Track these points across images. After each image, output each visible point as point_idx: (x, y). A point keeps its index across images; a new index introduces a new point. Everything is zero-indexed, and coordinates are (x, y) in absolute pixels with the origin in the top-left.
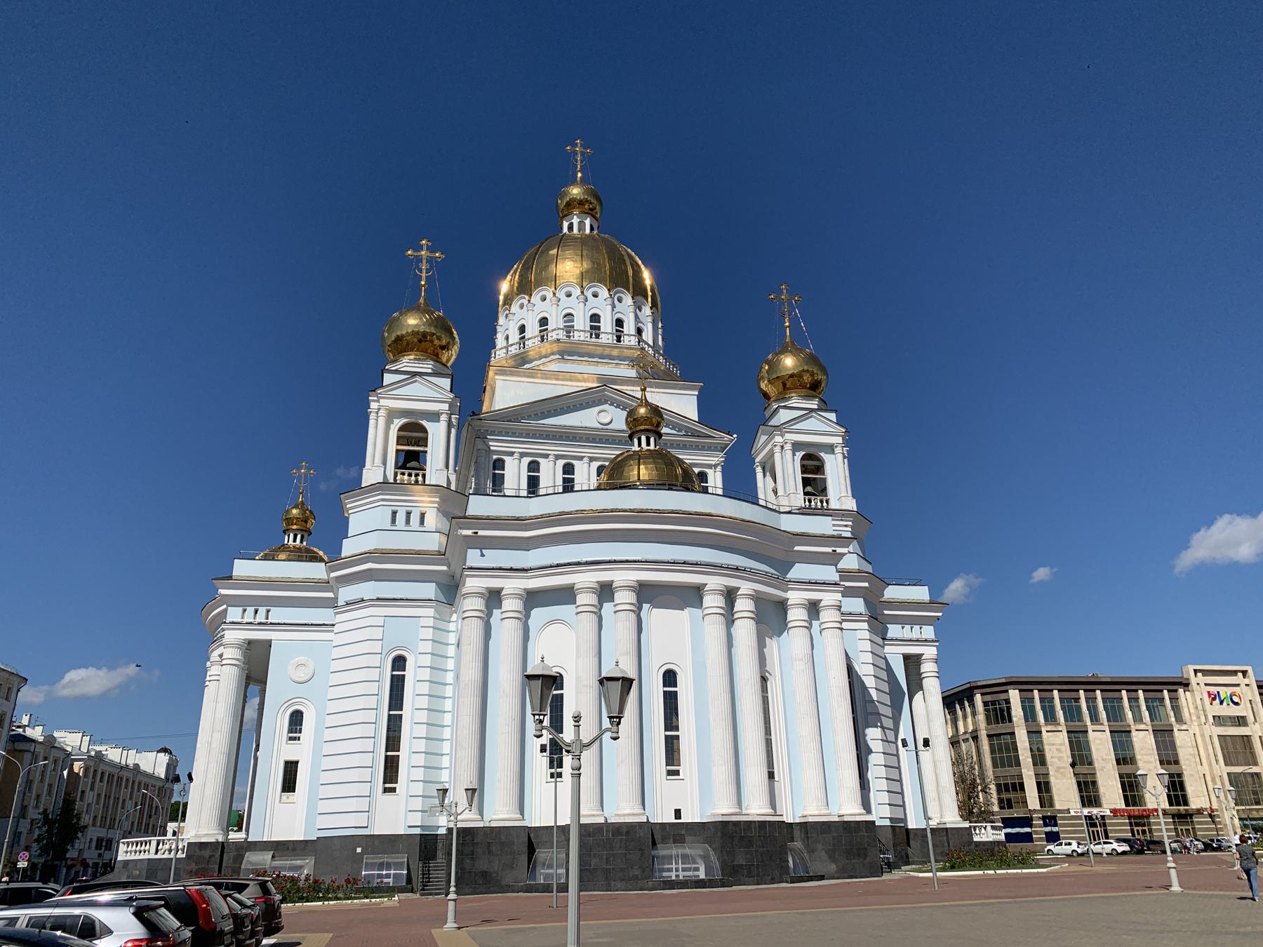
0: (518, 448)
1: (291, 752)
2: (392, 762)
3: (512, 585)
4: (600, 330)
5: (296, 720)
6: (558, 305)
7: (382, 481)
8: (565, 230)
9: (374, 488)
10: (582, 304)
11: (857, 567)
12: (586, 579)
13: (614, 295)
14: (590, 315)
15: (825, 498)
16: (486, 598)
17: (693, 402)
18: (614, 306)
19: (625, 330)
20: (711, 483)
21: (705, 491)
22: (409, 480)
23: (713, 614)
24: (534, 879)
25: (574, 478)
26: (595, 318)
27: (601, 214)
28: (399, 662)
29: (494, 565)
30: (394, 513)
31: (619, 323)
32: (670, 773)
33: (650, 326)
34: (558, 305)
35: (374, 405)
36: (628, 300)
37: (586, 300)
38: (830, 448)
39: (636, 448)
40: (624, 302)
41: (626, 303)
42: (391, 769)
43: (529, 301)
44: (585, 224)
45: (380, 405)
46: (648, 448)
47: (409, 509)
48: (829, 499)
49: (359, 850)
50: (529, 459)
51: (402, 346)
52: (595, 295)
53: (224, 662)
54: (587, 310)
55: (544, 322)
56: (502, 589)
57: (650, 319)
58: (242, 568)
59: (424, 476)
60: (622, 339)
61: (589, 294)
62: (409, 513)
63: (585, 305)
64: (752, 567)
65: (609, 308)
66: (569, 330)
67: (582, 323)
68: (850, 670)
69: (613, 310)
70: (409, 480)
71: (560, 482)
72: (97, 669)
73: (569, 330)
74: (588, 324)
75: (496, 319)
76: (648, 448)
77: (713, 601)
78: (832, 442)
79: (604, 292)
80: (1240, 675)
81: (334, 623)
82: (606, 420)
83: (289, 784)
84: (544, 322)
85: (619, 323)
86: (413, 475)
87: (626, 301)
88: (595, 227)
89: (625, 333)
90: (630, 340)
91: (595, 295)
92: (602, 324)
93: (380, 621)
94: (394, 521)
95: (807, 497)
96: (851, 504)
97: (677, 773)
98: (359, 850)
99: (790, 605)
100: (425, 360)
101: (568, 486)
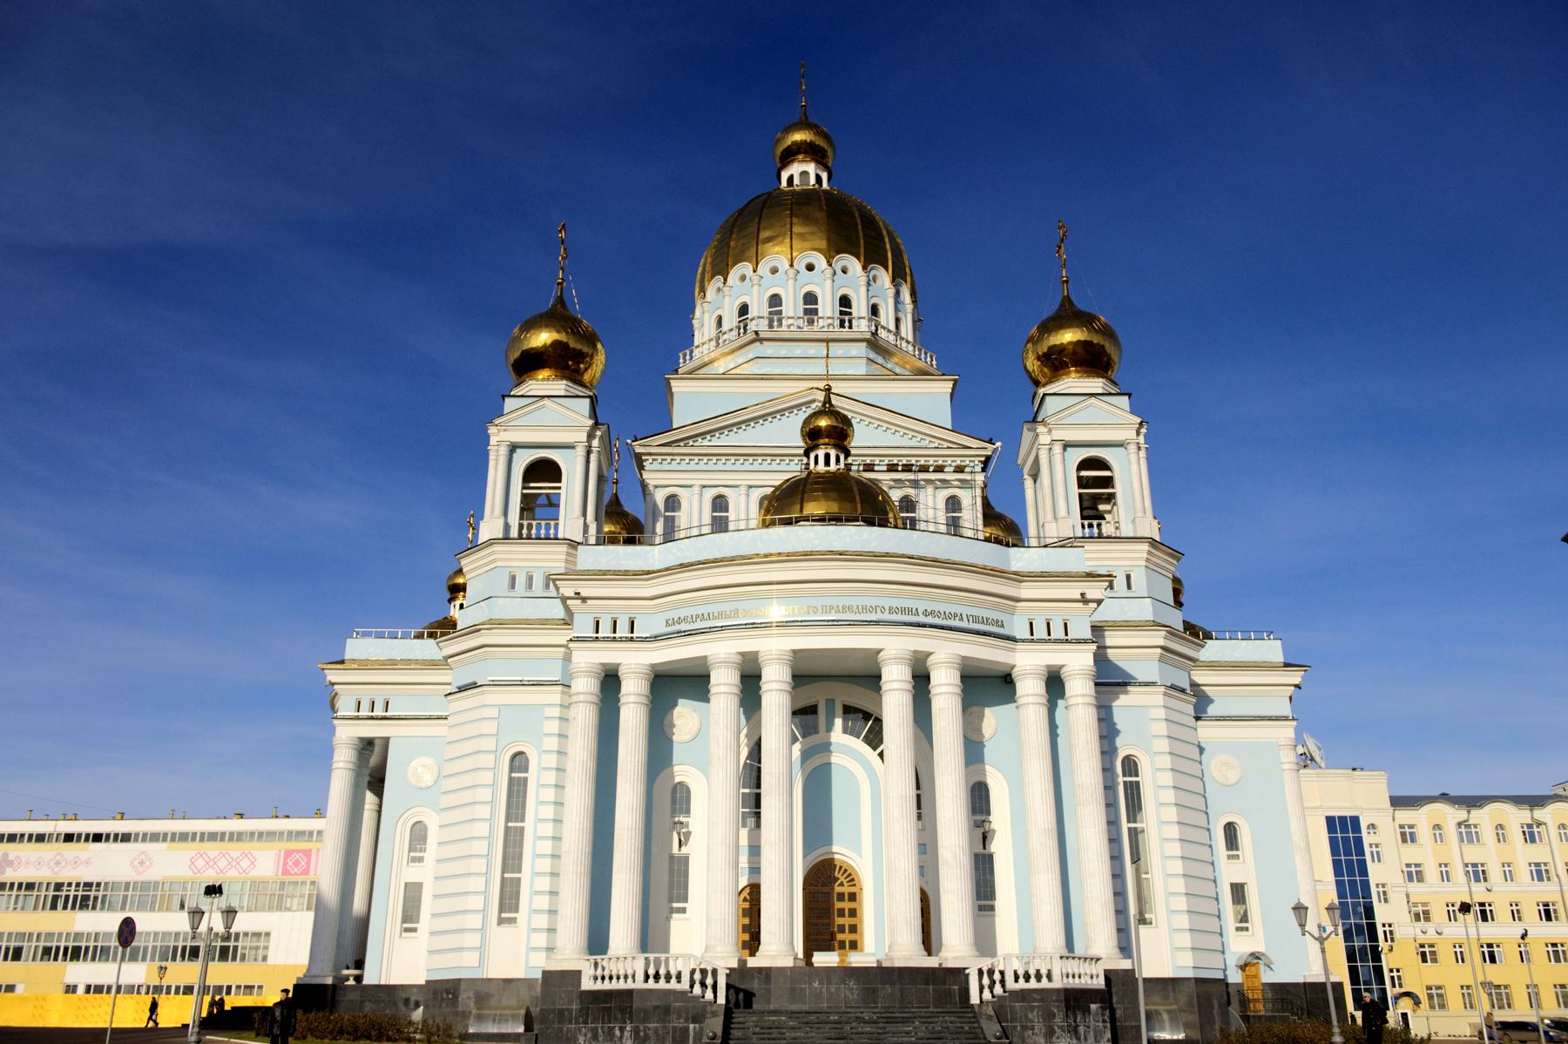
0: (697, 480)
1: (413, 874)
2: (1232, 844)
4: (816, 313)
5: (1231, 831)
6: (760, 285)
7: (501, 536)
8: (784, 183)
9: (491, 542)
14: (802, 294)
19: (854, 311)
20: (921, 513)
21: (912, 524)
22: (1091, 532)
25: (727, 517)
27: (834, 160)
34: (760, 285)
35: (493, 441)
36: (884, 277)
42: (509, 899)
45: (499, 437)
46: (827, 468)
50: (714, 492)
51: (528, 364)
52: (810, 268)
55: (775, 300)
58: (357, 648)
59: (556, 526)
63: (834, 281)
65: (829, 282)
70: (1091, 532)
71: (707, 519)
72: (1117, 735)
74: (801, 307)
75: (693, 312)
79: (854, 265)
81: (444, 714)
83: (410, 915)
84: (775, 300)
86: (1095, 526)
88: (824, 176)
90: (862, 327)
92: (820, 306)
93: (494, 712)
94: (513, 586)
95: (1086, 523)
96: (1150, 528)
101: (720, 525)
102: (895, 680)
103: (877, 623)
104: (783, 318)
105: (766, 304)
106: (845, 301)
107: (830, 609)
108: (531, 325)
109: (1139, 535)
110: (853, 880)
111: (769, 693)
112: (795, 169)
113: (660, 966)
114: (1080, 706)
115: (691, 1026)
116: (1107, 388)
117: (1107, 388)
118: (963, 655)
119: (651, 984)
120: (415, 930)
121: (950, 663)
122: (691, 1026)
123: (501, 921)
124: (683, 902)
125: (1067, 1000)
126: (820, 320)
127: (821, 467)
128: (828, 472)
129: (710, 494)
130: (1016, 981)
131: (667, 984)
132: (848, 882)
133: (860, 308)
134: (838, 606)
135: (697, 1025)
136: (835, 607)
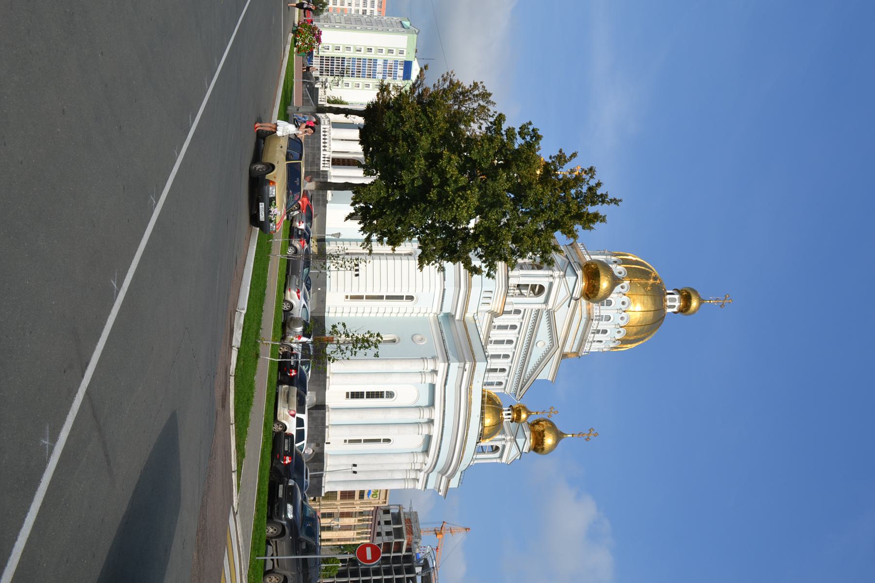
0: (510, 379)
3: (439, 381)
12: (437, 415)
29: (449, 374)
30: (491, 292)
32: (348, 393)
38: (501, 457)
43: (624, 295)
47: (493, 292)
49: (319, 289)
61: (621, 329)
62: (490, 298)
67: (602, 325)
77: (420, 458)
78: (503, 458)
80: (385, 501)
82: (538, 345)
97: (347, 397)
98: (319, 289)
106: (605, 332)
130: (323, 128)
133: (599, 337)
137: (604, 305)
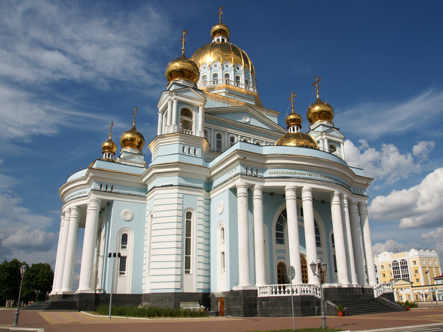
10: (209, 71)
11: (202, 165)
13: (224, 64)
14: (213, 74)
15: (191, 131)
16: (295, 191)
17: (254, 103)
18: (223, 68)
23: (240, 196)
24: (336, 281)
26: (215, 75)
28: (189, 215)
31: (237, 78)
33: (243, 75)
37: (211, 68)
39: (292, 132)
40: (229, 66)
41: (241, 70)
44: (224, 40)
46: (294, 132)
48: (192, 132)
53: (65, 219)
54: (212, 72)
56: (285, 186)
57: (243, 72)
60: (239, 85)
63: (211, 70)
64: (243, 172)
65: (221, 70)
66: (227, 82)
68: (131, 230)
69: (223, 70)
73: (227, 82)
76: (294, 132)
85: (227, 76)
87: (241, 69)
89: (240, 83)
91: (227, 66)
99: (303, 190)
100: (324, 121)
102: (290, 195)
103: (280, 178)
104: (218, 80)
105: (212, 76)
107: (282, 173)
108: (313, 106)
109: (290, 145)
110: (305, 262)
111: (304, 201)
112: (216, 39)
113: (277, 288)
114: (345, 207)
115: (316, 307)
116: (194, 87)
117: (194, 87)
118: (312, 187)
119: (274, 295)
120: (124, 274)
121: (258, 188)
122: (316, 307)
123: (121, 274)
124: (124, 271)
125: (321, 314)
126: (240, 85)
127: (292, 132)
128: (294, 133)
129: (217, 132)
131: (289, 294)
132: (304, 262)
134: (284, 172)
135: (317, 307)
136: (283, 172)
137: (218, 79)
